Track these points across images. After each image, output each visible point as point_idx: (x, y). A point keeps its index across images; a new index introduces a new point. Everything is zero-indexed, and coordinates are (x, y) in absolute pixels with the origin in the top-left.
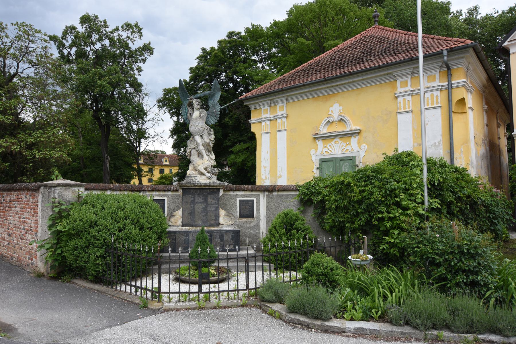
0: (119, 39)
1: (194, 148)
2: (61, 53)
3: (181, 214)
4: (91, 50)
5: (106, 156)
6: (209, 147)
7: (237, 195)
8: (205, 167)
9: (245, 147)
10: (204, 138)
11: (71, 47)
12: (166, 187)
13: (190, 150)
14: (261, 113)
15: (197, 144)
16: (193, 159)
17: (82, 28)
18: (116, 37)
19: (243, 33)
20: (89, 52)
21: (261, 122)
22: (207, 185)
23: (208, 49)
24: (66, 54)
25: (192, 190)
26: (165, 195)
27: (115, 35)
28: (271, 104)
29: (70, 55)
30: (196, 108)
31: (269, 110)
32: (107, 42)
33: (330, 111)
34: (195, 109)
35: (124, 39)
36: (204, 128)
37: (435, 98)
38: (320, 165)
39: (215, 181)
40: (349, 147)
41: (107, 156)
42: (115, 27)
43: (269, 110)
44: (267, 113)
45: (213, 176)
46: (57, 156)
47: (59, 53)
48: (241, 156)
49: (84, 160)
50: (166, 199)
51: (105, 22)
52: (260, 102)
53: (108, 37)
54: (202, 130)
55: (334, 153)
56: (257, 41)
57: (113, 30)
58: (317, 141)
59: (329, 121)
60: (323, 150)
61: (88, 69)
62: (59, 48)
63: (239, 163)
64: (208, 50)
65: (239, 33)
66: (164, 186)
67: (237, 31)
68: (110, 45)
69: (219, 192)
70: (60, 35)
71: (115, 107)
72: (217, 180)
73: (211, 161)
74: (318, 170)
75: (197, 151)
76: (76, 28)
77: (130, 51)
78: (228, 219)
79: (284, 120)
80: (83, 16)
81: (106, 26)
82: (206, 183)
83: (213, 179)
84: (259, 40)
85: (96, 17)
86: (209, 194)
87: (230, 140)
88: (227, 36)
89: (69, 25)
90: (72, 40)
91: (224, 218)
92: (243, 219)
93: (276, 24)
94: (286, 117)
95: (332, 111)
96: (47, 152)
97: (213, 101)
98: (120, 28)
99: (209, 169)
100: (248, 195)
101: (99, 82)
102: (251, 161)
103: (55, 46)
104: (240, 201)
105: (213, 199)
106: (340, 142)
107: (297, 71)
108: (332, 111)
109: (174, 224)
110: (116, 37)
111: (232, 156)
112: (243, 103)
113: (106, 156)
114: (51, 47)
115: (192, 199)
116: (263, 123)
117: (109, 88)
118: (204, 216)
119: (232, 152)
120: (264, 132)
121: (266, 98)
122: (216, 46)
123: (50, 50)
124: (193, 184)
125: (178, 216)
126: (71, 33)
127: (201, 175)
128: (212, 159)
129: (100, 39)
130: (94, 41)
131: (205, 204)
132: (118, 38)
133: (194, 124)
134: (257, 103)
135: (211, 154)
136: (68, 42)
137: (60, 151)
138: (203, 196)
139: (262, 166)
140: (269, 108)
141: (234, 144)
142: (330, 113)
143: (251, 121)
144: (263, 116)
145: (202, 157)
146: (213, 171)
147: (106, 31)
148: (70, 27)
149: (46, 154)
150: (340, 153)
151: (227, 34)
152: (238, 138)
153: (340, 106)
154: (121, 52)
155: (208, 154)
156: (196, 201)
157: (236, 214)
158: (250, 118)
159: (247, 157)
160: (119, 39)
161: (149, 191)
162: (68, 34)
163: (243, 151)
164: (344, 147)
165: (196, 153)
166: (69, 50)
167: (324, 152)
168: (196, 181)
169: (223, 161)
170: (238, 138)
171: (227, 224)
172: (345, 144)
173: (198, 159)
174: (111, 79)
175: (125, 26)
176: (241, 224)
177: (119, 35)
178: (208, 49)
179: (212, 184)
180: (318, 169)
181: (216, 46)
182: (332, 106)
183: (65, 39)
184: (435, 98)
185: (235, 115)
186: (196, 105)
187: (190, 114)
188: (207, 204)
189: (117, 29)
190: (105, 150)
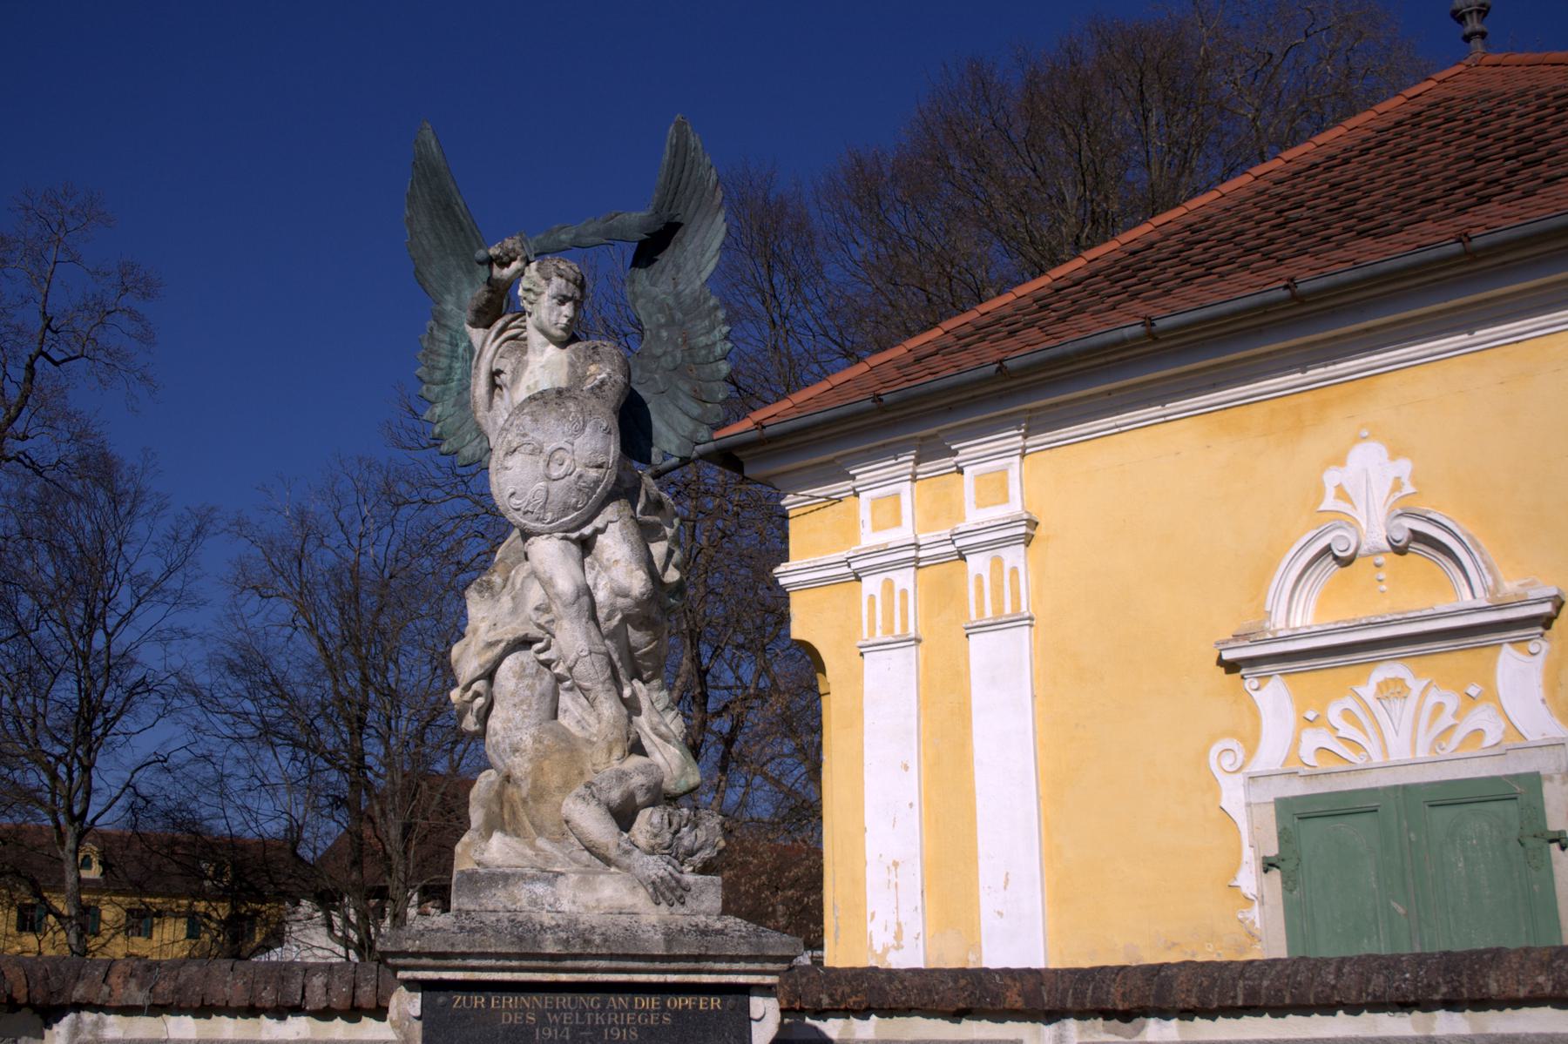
31: (1014, 474)
33: (1330, 492)
37: (1007, 577)
38: (1284, 837)
40: (1482, 718)
55: (1377, 759)
58: (1251, 684)
59: (1328, 549)
60: (1296, 742)
74: (1275, 875)
79: (1013, 556)
94: (1028, 540)
95: (1340, 488)
106: (1416, 685)
107: (986, 320)
108: (1340, 488)
120: (879, 636)
142: (1329, 503)
143: (786, 574)
150: (1422, 754)
153: (1395, 454)
158: (784, 556)
164: (1446, 720)
167: (1310, 759)
172: (1451, 702)
180: (1268, 865)
182: (1340, 460)
184: (1007, 577)
187: (494, 374)
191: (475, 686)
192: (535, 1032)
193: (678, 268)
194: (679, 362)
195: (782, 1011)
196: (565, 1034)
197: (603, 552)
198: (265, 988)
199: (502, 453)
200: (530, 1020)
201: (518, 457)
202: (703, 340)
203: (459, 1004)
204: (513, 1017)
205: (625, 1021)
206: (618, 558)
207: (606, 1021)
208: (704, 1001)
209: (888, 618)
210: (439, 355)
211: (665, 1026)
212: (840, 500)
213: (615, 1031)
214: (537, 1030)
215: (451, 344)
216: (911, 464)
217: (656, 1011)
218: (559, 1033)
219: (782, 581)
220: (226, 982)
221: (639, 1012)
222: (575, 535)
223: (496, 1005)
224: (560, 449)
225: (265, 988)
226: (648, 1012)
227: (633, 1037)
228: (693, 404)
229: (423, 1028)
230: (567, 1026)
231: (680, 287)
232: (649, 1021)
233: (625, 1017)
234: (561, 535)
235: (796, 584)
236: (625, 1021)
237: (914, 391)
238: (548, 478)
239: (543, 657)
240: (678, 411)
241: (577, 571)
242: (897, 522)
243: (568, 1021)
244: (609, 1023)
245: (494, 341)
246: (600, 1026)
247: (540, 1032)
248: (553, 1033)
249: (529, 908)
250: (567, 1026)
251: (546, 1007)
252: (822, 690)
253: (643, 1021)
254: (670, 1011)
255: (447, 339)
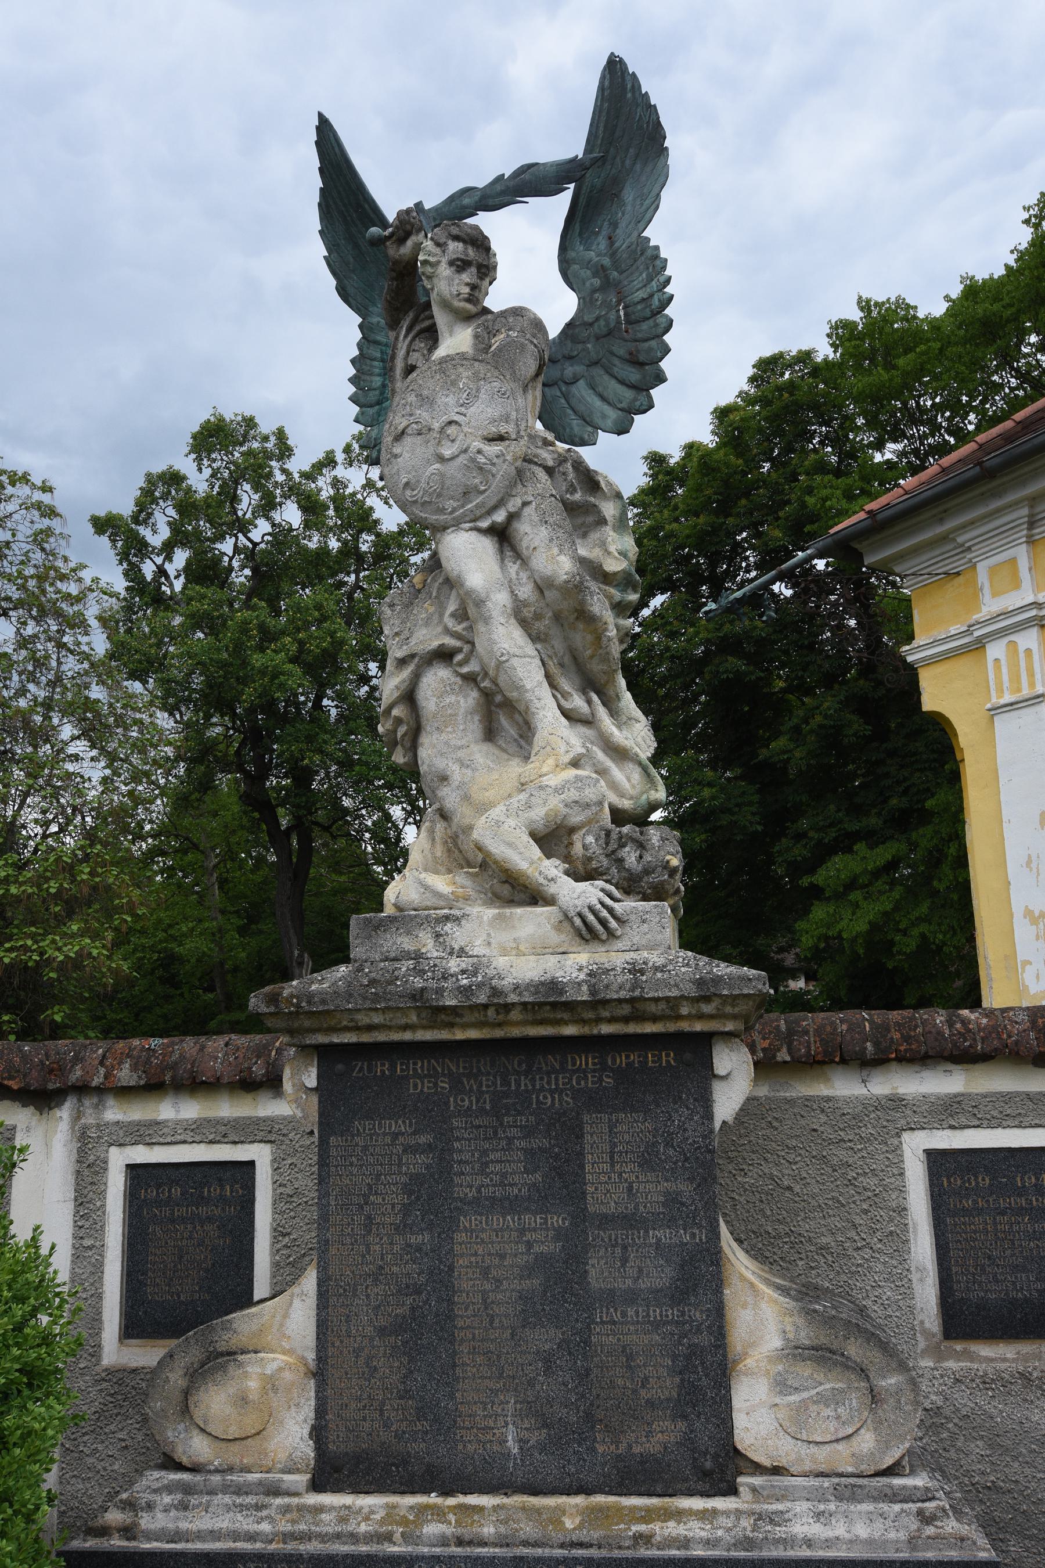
0: (338, 500)
1: (443, 656)
2: (133, 573)
3: (311, 1340)
4: (236, 550)
5: (296, 953)
6: (581, 638)
7: (896, 1102)
8: (538, 814)
9: (880, 862)
10: (524, 545)
11: (168, 549)
12: (261, 1052)
13: (406, 673)
14: (977, 591)
15: (461, 615)
16: (440, 764)
17: (200, 470)
18: (327, 493)
19: (824, 351)
20: (231, 559)
21: (978, 646)
22: (570, 1006)
23: (675, 456)
24: (149, 577)
25: (420, 1066)
26: (258, 1121)
27: (321, 482)
28: (1032, 524)
29: (163, 580)
30: (446, 305)
31: (1023, 564)
32: (291, 514)
34: (441, 318)
35: (354, 494)
36: (519, 448)
39: (655, 958)
41: (301, 956)
42: (321, 455)
43: (1023, 564)
44: (1017, 584)
45: (626, 906)
46: (66, 956)
47: (126, 574)
48: (864, 904)
49: (229, 977)
50: (260, 1154)
51: (281, 435)
52: (963, 527)
53: (293, 490)
54: (503, 470)
56: (895, 367)
57: (313, 466)
61: (221, 616)
62: (124, 556)
63: (854, 940)
64: (672, 461)
65: (805, 357)
66: (241, 1040)
67: (793, 347)
68: (307, 525)
69: (706, 1074)
70: (126, 508)
71: (321, 752)
72: (684, 945)
73: (617, 774)
75: (470, 679)
76: (184, 478)
77: (378, 535)
78: (833, 1399)
80: (202, 427)
81: (285, 451)
82: (553, 986)
83: (634, 935)
84: (901, 362)
85: (250, 423)
86: (594, 1101)
87: (800, 836)
88: (752, 380)
89: (158, 467)
90: (169, 524)
91: (781, 1386)
92: (985, 1350)
93: (973, 291)
96: (29, 942)
97: (602, 244)
98: (340, 457)
99: (586, 842)
100: (1008, 1097)
101: (257, 660)
102: (913, 925)
103: (113, 552)
104: (935, 1158)
105: (648, 1162)
109: (234, 1455)
110: (327, 493)
111: (819, 912)
112: (859, 558)
113: (296, 953)
114: (66, 531)
115: (418, 1163)
116: (995, 651)
117: (296, 679)
118: (548, 1361)
119: (816, 893)
120: (1007, 698)
121: (996, 494)
122: (705, 435)
123: (63, 542)
124: (418, 995)
125: (274, 1361)
126: (165, 496)
127: (511, 902)
128: (620, 754)
129: (267, 506)
130: (249, 515)
131: (556, 1221)
132: (332, 492)
133: (423, 415)
134: (944, 539)
135: (610, 703)
136: (157, 534)
137: (82, 933)
138: (529, 1132)
139: (1018, 909)
140: (1022, 553)
141: (823, 853)
144: (991, 605)
145: (526, 730)
146: (630, 856)
147: (284, 471)
148: (162, 476)
149: (26, 949)
151: (751, 372)
152: (841, 822)
154: (345, 543)
155: (578, 702)
156: (466, 1186)
157: (908, 1293)
159: (896, 908)
160: (338, 500)
161: (125, 1092)
162: (155, 501)
163: (870, 884)
165: (468, 700)
166: (159, 560)
168: (454, 965)
169: (781, 950)
170: (841, 822)
171: (822, 1457)
173: (481, 754)
174: (301, 643)
175: (356, 446)
176: (962, 1399)
177: (336, 483)
178: (675, 456)
179: (619, 986)
181: (705, 435)
183: (145, 522)
185: (818, 719)
186: (444, 271)
188: (580, 1216)
189: (329, 461)
190: (292, 931)
191: (395, 712)
192: (449, 1101)
193: (614, 225)
194: (612, 325)
195: (756, 1064)
196: (485, 1102)
197: (521, 540)
198: (256, 1063)
199: (390, 439)
200: (443, 1088)
201: (408, 440)
202: (641, 294)
203: (360, 1071)
204: (423, 1084)
205: (557, 1084)
206: (536, 544)
207: (534, 1086)
208: (653, 1056)
209: (1015, 678)
210: (371, 375)
211: (605, 1088)
212: (958, 574)
213: (545, 1097)
214: (452, 1099)
215: (383, 361)
216: (1025, 532)
217: (594, 1071)
218: (477, 1102)
219: (909, 659)
220: (217, 1058)
221: (574, 1072)
222: (485, 524)
223: (402, 1070)
224: (450, 423)
225: (256, 1063)
226: (585, 1071)
227: (568, 1104)
228: (630, 369)
229: (320, 1102)
230: (487, 1092)
231: (617, 244)
232: (586, 1083)
233: (557, 1079)
234: (468, 525)
235: (923, 659)
236: (557, 1084)
237: (1018, 450)
238: (441, 459)
239: (465, 670)
240: (613, 382)
241: (496, 567)
242: (1017, 584)
243: (488, 1086)
244: (538, 1087)
245: (406, 337)
246: (527, 1091)
247: (455, 1101)
248: (471, 1102)
249: (435, 954)
250: (487, 1092)
251: (461, 1071)
252: (959, 758)
253: (578, 1083)
254: (612, 1070)
255: (379, 355)
